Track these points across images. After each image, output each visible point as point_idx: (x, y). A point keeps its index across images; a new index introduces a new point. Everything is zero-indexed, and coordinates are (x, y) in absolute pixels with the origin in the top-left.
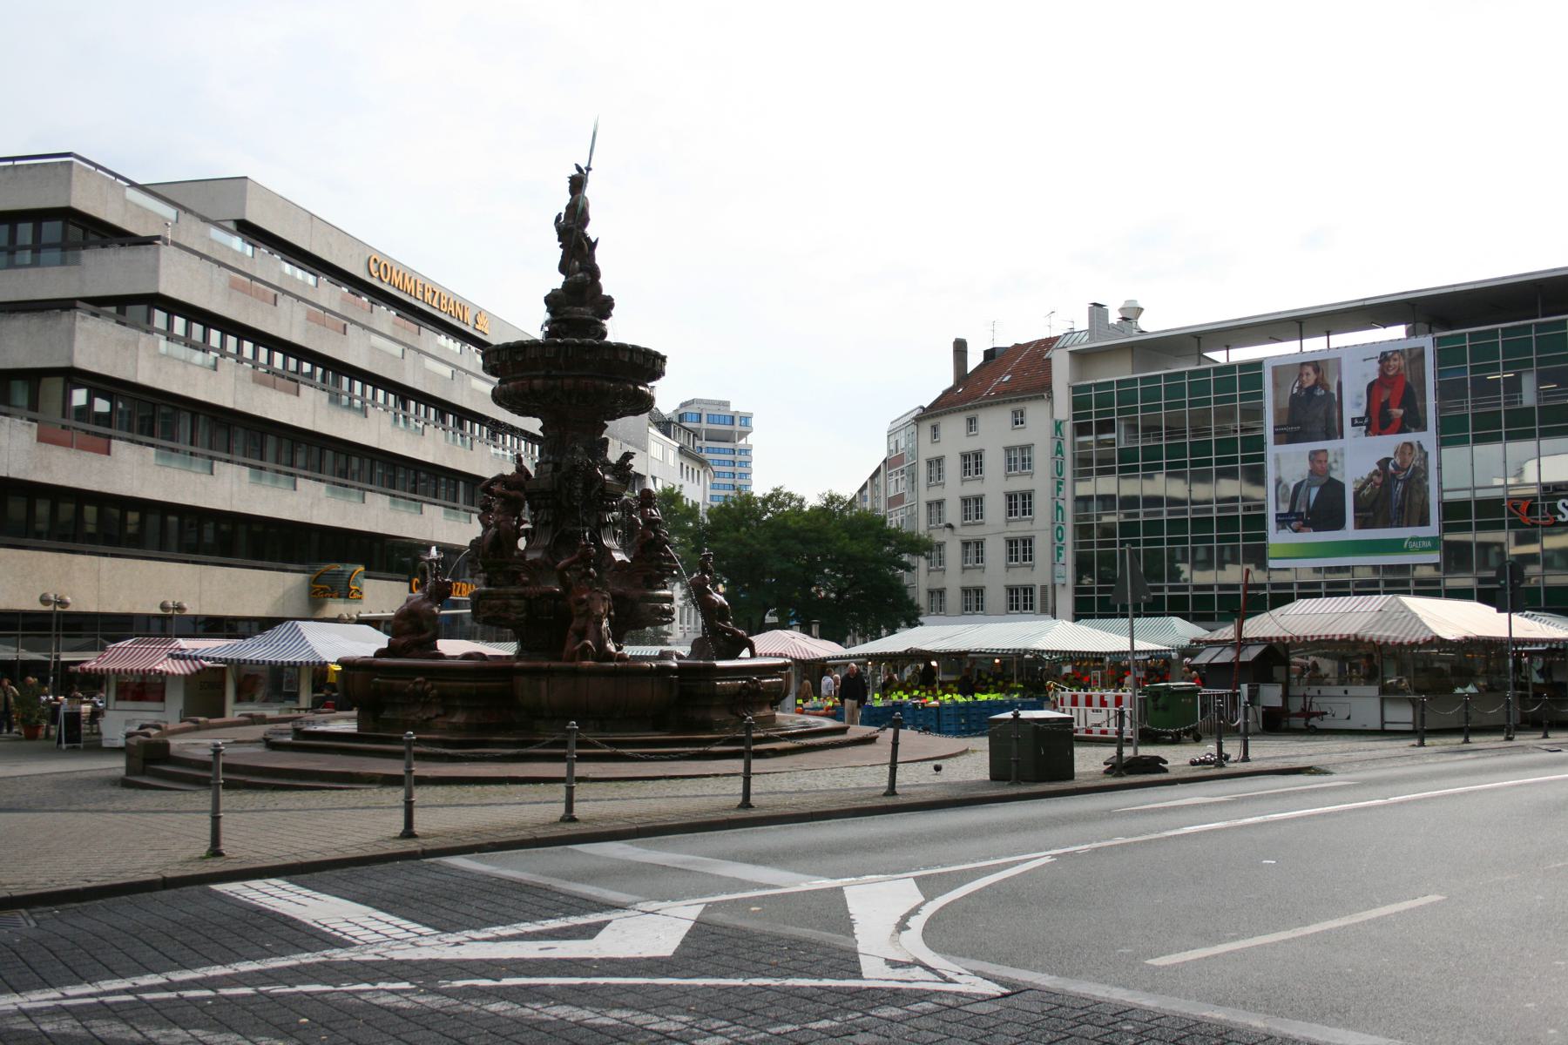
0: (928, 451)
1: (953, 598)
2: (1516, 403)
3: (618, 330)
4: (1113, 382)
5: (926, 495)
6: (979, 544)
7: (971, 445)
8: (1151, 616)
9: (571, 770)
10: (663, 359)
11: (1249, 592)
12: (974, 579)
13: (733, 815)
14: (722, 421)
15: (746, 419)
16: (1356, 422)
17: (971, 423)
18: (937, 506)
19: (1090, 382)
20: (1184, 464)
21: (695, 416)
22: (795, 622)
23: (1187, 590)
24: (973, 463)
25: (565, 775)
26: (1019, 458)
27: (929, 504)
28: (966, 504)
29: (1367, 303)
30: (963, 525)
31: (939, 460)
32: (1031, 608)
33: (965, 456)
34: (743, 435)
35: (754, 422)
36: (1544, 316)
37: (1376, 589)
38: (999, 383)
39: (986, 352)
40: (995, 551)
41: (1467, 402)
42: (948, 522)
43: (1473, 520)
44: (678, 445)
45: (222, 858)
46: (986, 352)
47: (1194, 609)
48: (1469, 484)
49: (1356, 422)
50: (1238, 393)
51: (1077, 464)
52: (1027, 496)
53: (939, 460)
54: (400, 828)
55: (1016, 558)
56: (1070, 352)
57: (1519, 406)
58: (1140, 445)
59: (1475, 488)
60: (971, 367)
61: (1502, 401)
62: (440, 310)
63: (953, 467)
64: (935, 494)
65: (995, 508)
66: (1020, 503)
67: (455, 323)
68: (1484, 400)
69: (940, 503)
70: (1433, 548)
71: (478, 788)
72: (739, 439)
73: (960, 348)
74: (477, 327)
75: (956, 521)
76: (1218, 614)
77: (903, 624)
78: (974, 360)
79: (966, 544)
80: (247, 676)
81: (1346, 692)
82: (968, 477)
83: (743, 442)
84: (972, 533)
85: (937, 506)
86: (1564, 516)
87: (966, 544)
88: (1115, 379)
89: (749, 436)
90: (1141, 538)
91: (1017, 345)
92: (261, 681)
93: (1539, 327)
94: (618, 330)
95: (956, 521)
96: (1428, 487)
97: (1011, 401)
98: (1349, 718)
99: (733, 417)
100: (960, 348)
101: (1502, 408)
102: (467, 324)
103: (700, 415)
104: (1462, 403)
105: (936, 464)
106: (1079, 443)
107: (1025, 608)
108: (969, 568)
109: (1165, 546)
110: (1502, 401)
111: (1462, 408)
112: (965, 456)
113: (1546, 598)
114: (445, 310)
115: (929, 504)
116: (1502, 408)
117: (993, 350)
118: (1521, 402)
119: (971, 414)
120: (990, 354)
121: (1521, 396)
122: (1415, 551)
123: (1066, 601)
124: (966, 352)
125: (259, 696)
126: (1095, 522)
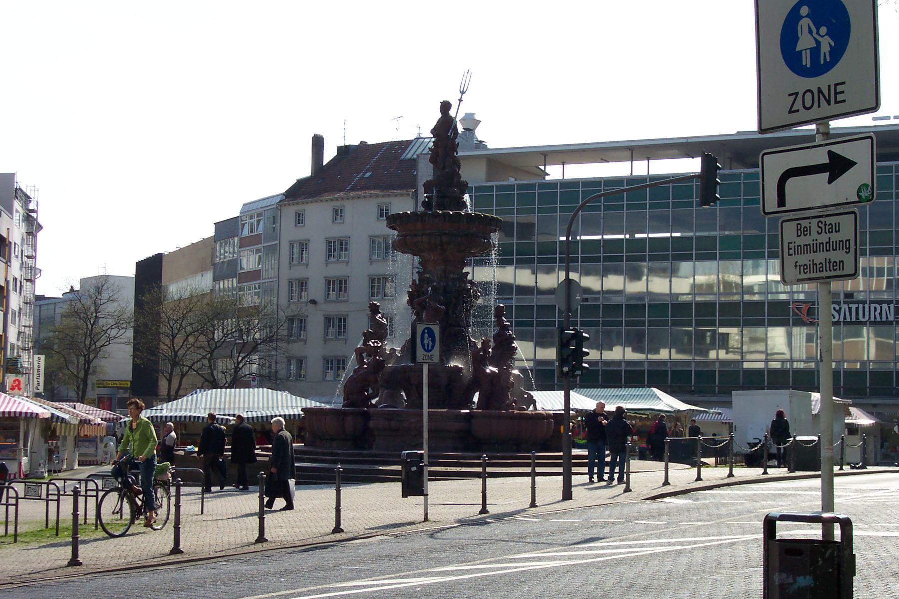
7: (337, 231)
9: (485, 470)
10: (338, 147)
13: (166, 559)
20: (620, 259)
22: (585, 365)
25: (428, 482)
29: (690, 140)
30: (326, 302)
45: (267, 542)
50: (625, 202)
54: (171, 545)
73: (318, 143)
75: (319, 297)
78: (329, 154)
84: (334, 310)
86: (834, 309)
91: (363, 144)
95: (319, 297)
96: (83, 281)
100: (318, 143)
119: (337, 204)
124: (323, 146)
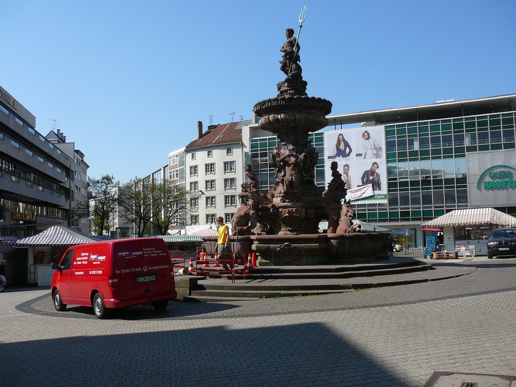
2: (463, 144)
3: (311, 92)
4: (267, 138)
11: (359, 212)
16: (357, 155)
23: (366, 211)
24: (210, 168)
26: (228, 166)
27: (191, 183)
28: (207, 183)
36: (464, 116)
37: (369, 212)
41: (396, 148)
43: (409, 188)
49: (357, 155)
52: (233, 180)
56: (250, 127)
57: (412, 150)
60: (204, 132)
61: (477, 142)
62: (2, 98)
65: (219, 184)
66: (210, 184)
67: (7, 104)
69: (196, 183)
70: (385, 198)
73: (200, 124)
74: (14, 107)
78: (205, 130)
79: (207, 198)
80: (39, 252)
81: (479, 242)
87: (207, 198)
88: (267, 137)
90: (398, 188)
92: (46, 254)
93: (442, 121)
94: (311, 92)
95: (204, 190)
97: (226, 145)
98: (480, 251)
100: (200, 124)
101: (408, 151)
102: (11, 105)
104: (412, 147)
106: (253, 160)
109: (432, 190)
110: (477, 142)
111: (394, 150)
114: (4, 98)
115: (191, 183)
116: (408, 151)
118: (413, 149)
119: (228, 147)
120: (210, 127)
121: (413, 147)
122: (378, 199)
125: (46, 260)
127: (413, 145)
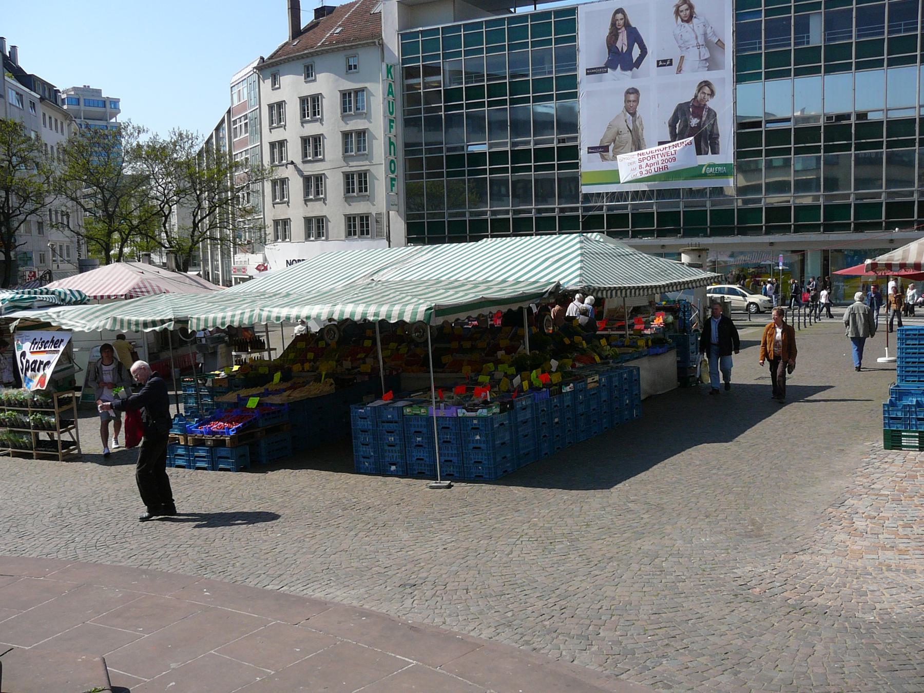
0: (269, 96)
1: (297, 227)
5: (269, 136)
6: (319, 178)
8: (497, 236)
12: (316, 209)
14: (96, 104)
15: (115, 102)
16: (660, 63)
17: (308, 70)
18: (279, 146)
19: (418, 29)
21: (74, 100)
31: (280, 105)
32: (368, 234)
33: (303, 100)
34: (114, 115)
35: (121, 105)
38: (332, 34)
39: (317, 11)
40: (334, 185)
41: (760, 43)
42: (290, 159)
44: (39, 97)
46: (317, 11)
47: (428, 234)
48: (883, 107)
49: (660, 63)
51: (406, 104)
53: (280, 105)
55: (353, 189)
58: (464, 86)
59: (888, 110)
63: (292, 111)
64: (278, 135)
65: (332, 147)
68: (777, 41)
69: (282, 143)
71: (310, 164)
72: (110, 119)
76: (428, 238)
77: (679, 359)
82: (307, 118)
83: (113, 120)
84: (311, 169)
85: (279, 146)
88: (440, 26)
89: (118, 116)
99: (105, 101)
103: (78, 99)
104: (755, 43)
105: (277, 108)
106: (407, 85)
107: (362, 233)
108: (311, 200)
112: (303, 100)
113: (710, 221)
117: (323, 8)
120: (321, 12)
121: (808, 37)
123: (398, 226)
126: (805, 40)
127: (809, 33)
